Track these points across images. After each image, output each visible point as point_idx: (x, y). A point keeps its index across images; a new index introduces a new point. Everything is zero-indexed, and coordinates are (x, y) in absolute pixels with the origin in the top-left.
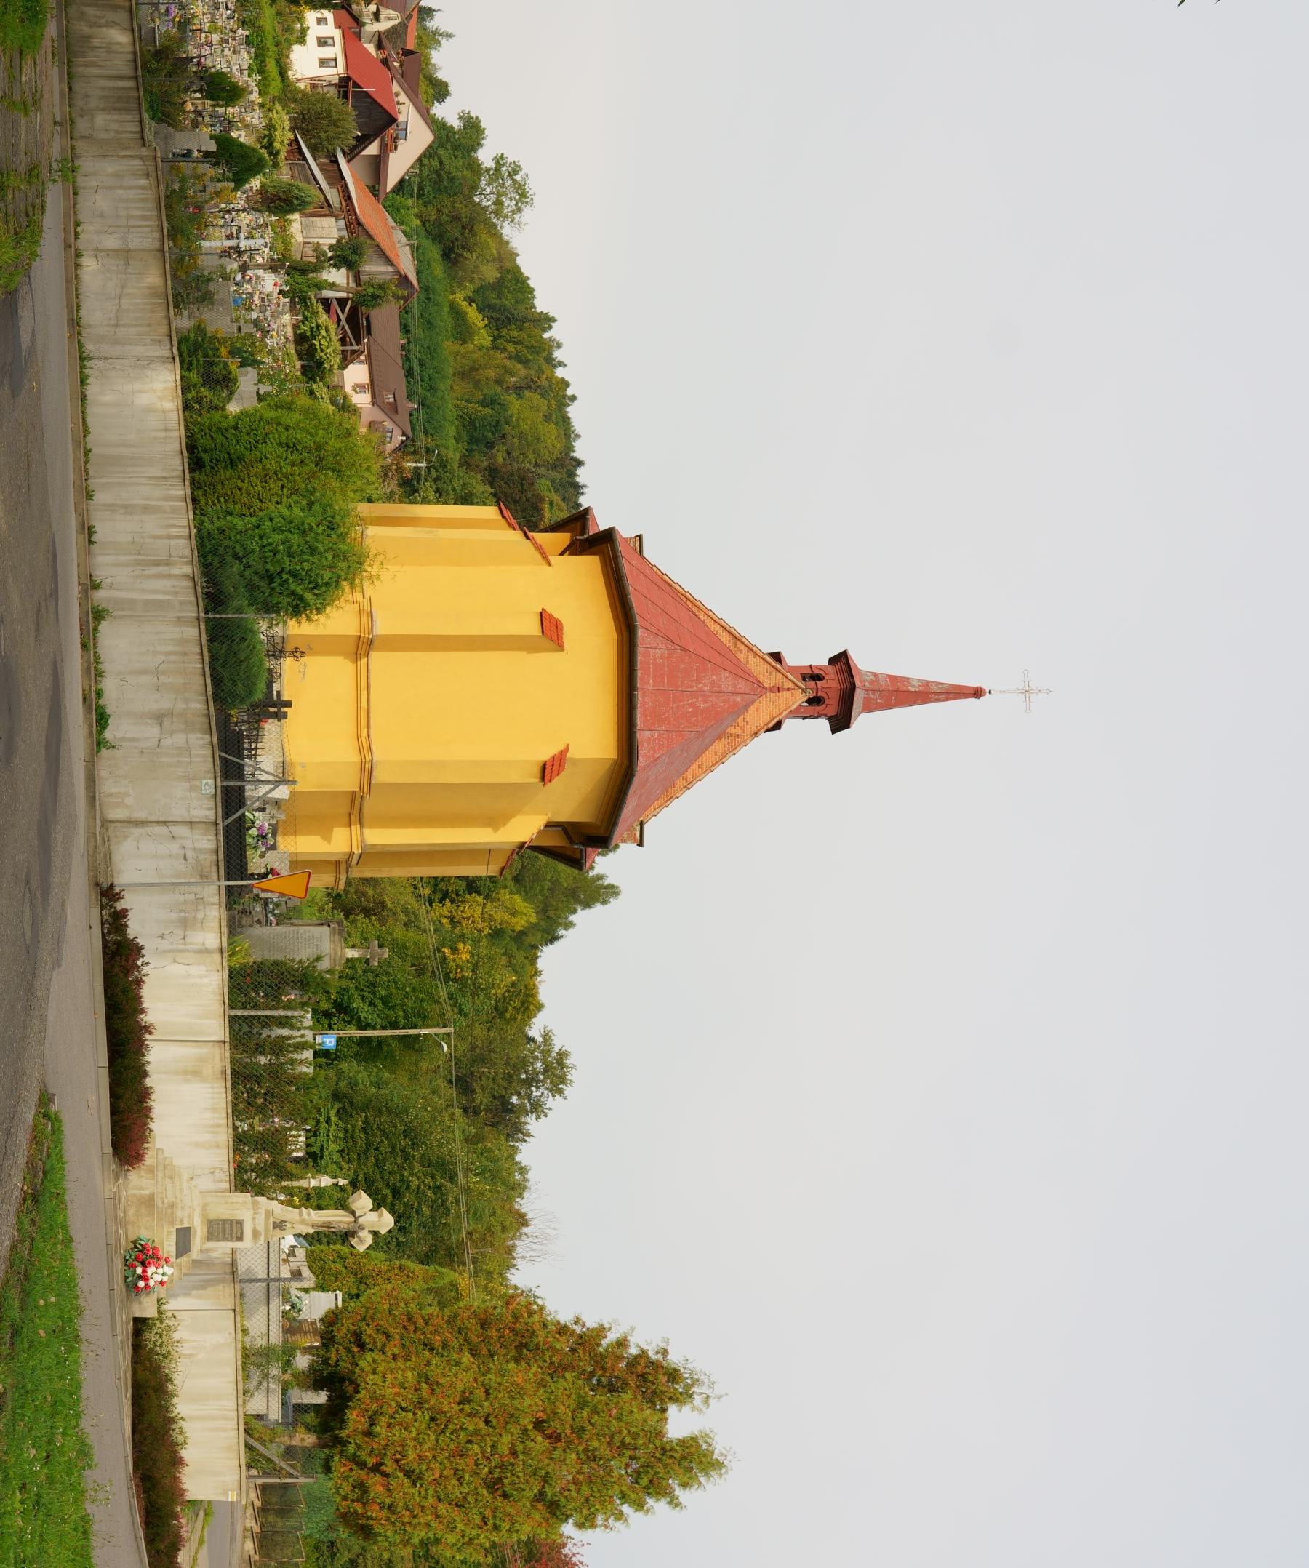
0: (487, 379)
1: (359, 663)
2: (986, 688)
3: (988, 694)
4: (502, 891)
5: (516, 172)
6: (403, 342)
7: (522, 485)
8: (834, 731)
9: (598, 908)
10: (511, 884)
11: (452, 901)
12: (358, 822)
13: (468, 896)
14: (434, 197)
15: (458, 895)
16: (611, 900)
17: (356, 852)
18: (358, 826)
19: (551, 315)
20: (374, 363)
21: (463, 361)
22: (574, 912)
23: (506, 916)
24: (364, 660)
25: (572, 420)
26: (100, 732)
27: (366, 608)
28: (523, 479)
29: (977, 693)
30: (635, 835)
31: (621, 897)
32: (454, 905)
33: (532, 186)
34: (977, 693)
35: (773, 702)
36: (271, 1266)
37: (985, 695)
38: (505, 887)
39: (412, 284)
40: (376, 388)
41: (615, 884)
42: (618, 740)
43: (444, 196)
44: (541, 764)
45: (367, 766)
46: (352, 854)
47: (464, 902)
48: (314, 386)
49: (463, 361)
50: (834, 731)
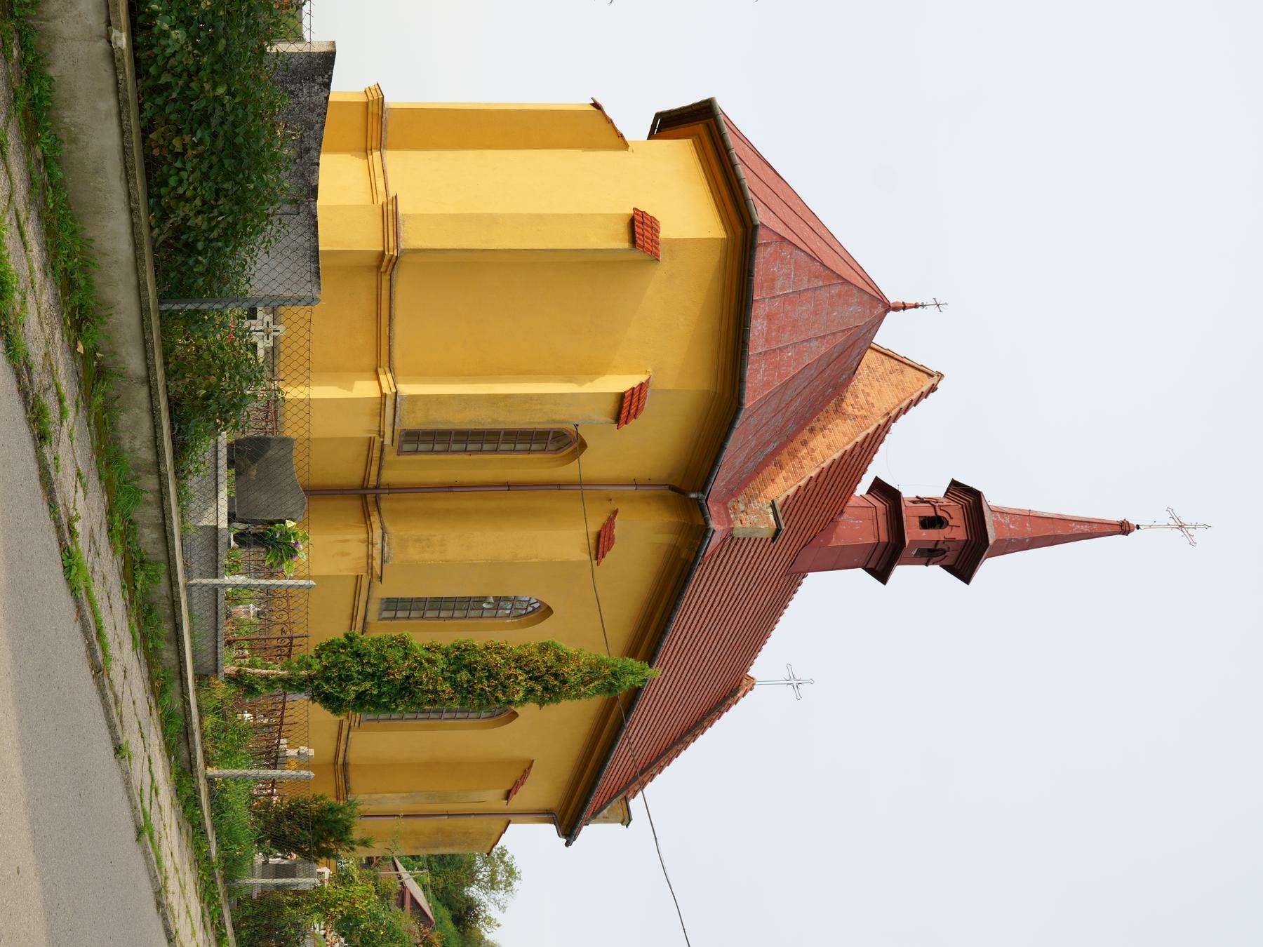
1: (370, 157)
2: (1133, 521)
3: (1136, 529)
5: (504, 855)
8: (967, 580)
12: (387, 369)
14: (440, 871)
17: (388, 392)
18: (389, 375)
24: (376, 154)
26: (59, 397)
27: (375, 111)
29: (1124, 528)
30: (768, 518)
33: (518, 865)
34: (1124, 528)
35: (896, 386)
37: (1133, 530)
39: (430, 918)
42: (723, 222)
43: (448, 869)
44: (627, 220)
45: (390, 207)
46: (384, 396)
50: (967, 580)
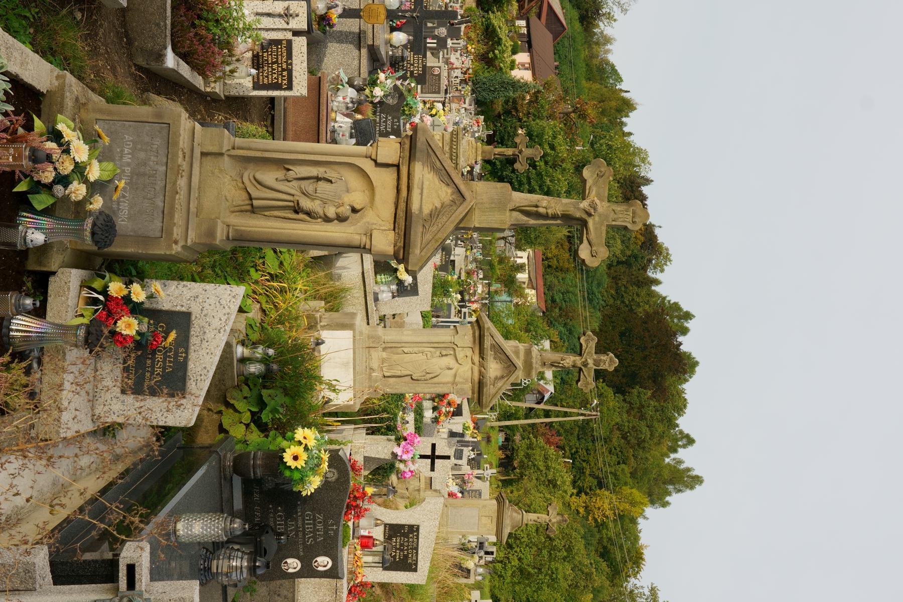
0: (611, 108)
4: (624, 488)
6: (556, 63)
7: (632, 187)
9: (688, 493)
10: (629, 480)
11: (586, 494)
13: (598, 491)
15: (591, 490)
16: (697, 486)
19: (685, 307)
20: (536, 69)
21: (594, 94)
22: (669, 494)
23: (627, 506)
25: (694, 355)
28: (633, 183)
31: (703, 484)
32: (588, 497)
36: (371, 30)
38: (626, 484)
40: (536, 65)
41: (700, 475)
47: (595, 494)
48: (491, 16)
49: (594, 94)
